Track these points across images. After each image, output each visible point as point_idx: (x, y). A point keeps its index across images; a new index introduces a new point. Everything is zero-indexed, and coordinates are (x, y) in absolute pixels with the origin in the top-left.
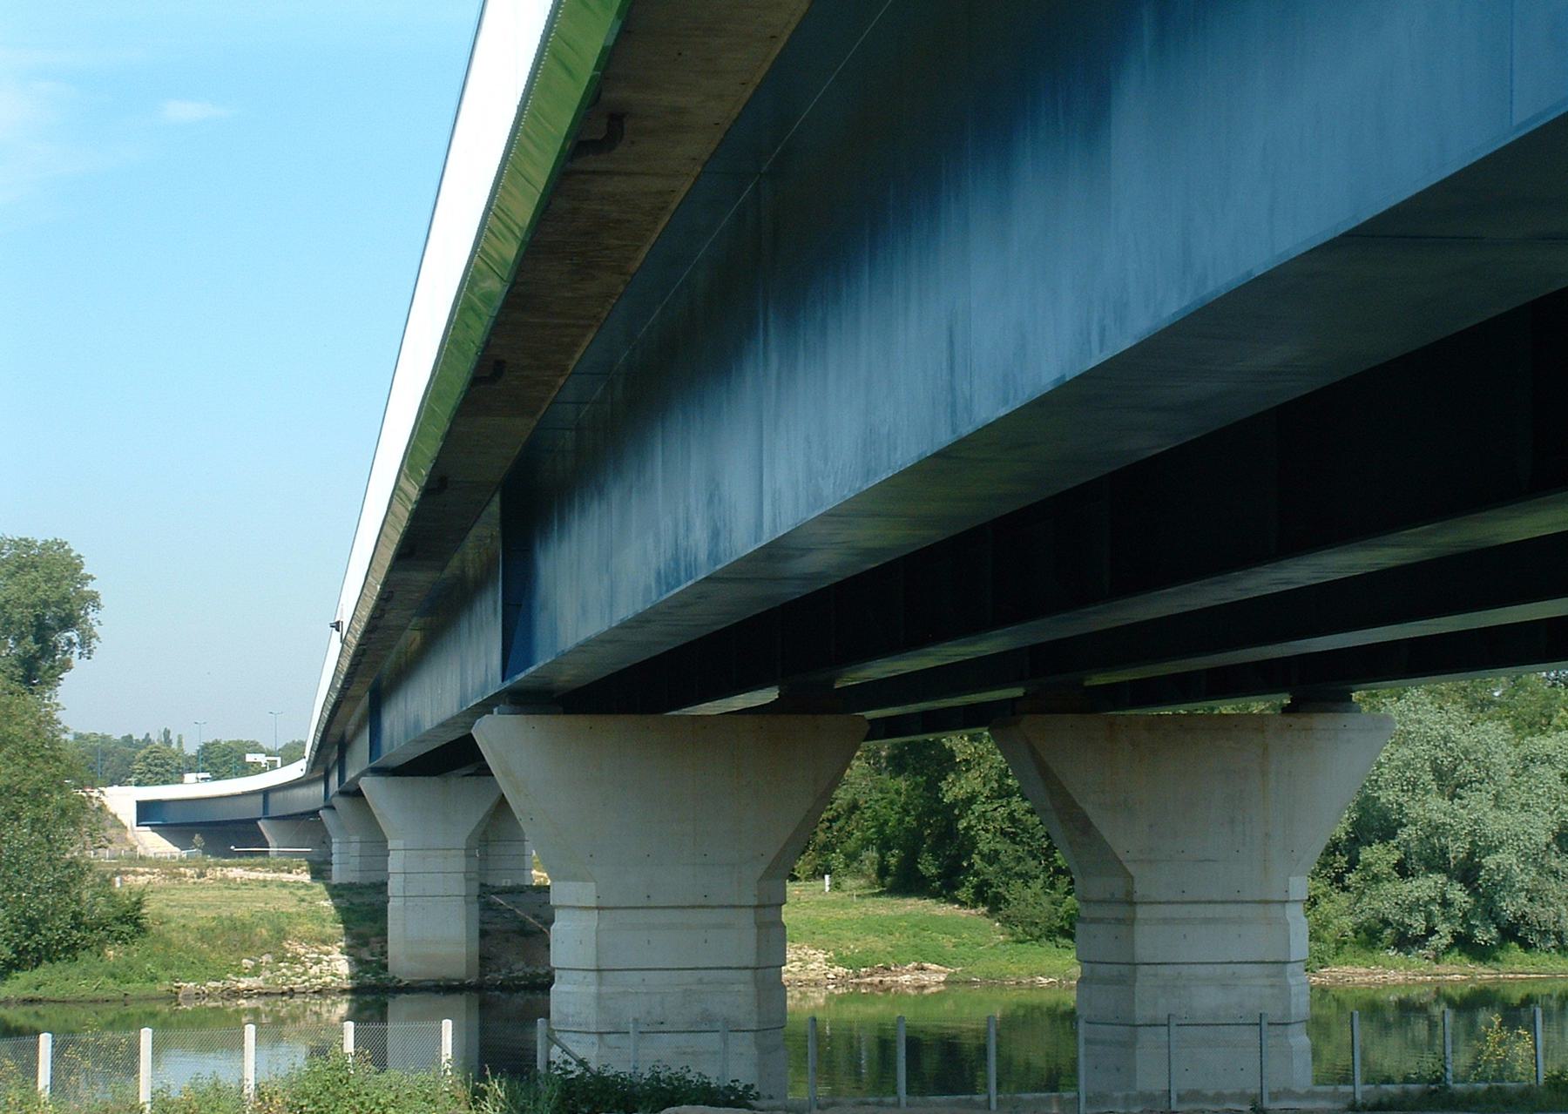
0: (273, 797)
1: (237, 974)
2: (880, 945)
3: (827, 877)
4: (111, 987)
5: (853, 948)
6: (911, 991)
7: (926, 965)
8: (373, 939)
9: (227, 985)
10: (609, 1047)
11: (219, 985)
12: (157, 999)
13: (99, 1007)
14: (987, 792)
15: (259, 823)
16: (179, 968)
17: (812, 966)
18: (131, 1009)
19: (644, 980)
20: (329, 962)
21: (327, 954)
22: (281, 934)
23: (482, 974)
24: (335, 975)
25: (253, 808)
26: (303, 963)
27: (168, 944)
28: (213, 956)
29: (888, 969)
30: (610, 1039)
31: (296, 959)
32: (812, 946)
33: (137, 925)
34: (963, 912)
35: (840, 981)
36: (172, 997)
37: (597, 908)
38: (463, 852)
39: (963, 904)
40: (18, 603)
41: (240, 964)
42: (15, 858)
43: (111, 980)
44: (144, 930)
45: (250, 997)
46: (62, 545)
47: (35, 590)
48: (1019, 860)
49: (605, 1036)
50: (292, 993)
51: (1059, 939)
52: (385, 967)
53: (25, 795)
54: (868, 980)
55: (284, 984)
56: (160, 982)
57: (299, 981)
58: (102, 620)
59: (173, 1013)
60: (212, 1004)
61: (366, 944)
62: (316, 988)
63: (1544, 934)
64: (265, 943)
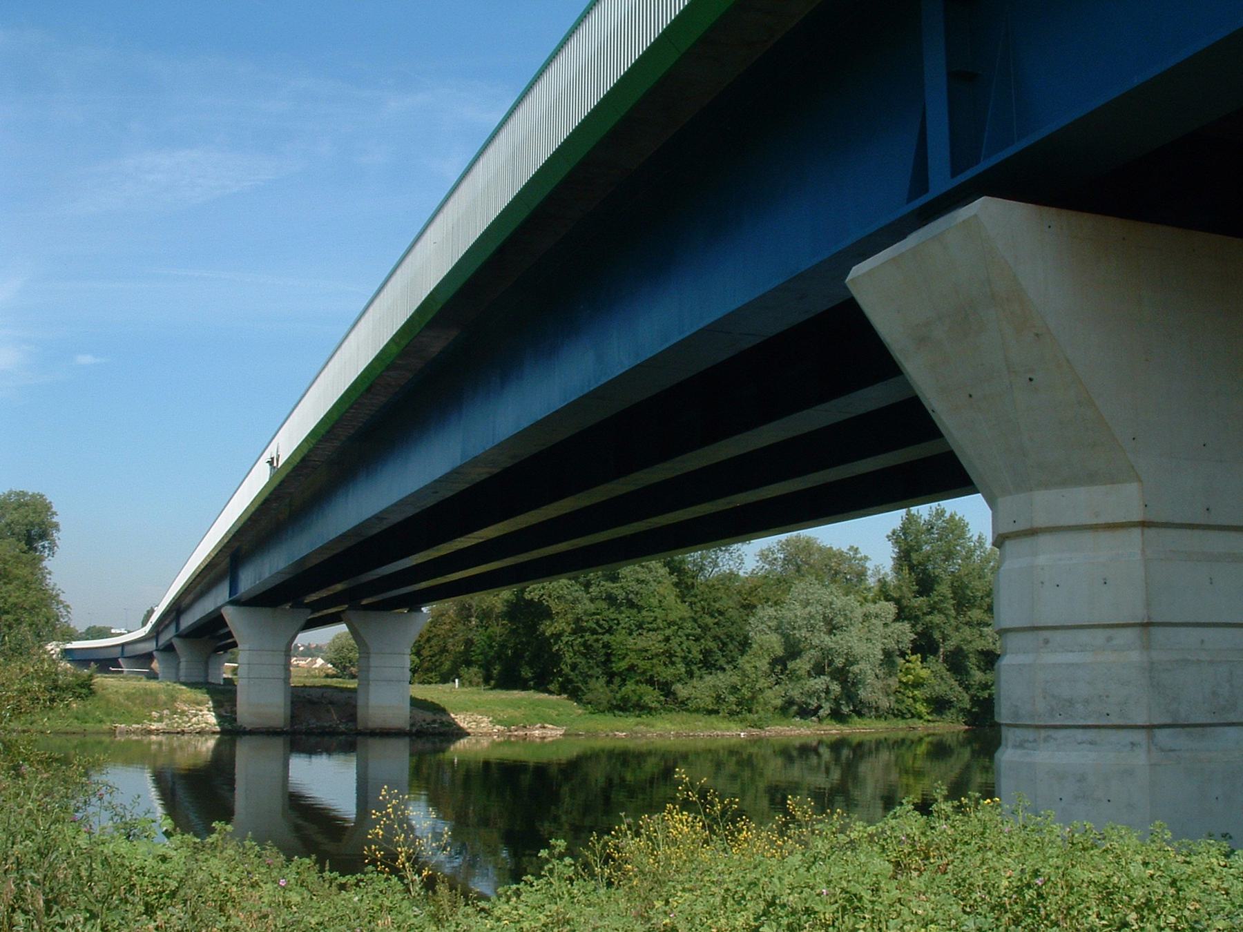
0: (127, 648)
1: (150, 720)
2: (517, 714)
3: (457, 680)
4: (76, 725)
5: (504, 716)
6: (538, 740)
7: (546, 725)
8: (226, 704)
9: (144, 727)
10: (1162, 750)
11: (139, 726)
12: (104, 733)
13: (69, 737)
14: (569, 630)
15: (120, 660)
16: (116, 716)
17: (482, 725)
18: (88, 739)
19: (1202, 641)
20: (203, 716)
21: (201, 711)
22: (173, 699)
23: (292, 726)
24: (207, 723)
25: (116, 653)
26: (187, 716)
27: (108, 701)
28: (135, 709)
29: (525, 727)
30: (1162, 736)
31: (183, 713)
32: (479, 714)
33: (90, 689)
34: (555, 697)
35: (500, 733)
36: (112, 732)
37: (1144, 524)
38: (283, 653)
39: (551, 693)
40: (18, 523)
41: (151, 715)
42: (20, 645)
43: (76, 721)
44: (94, 693)
45: (158, 734)
46: (42, 496)
47: (27, 516)
48: (591, 668)
49: (1157, 731)
50: (183, 733)
51: (616, 712)
52: (235, 720)
53: (25, 609)
54: (516, 733)
55: (177, 727)
56: (105, 723)
57: (187, 726)
58: (61, 538)
59: (112, 742)
60: (135, 738)
61: (222, 706)
62: (198, 730)
63: (870, 708)
64: (165, 703)
